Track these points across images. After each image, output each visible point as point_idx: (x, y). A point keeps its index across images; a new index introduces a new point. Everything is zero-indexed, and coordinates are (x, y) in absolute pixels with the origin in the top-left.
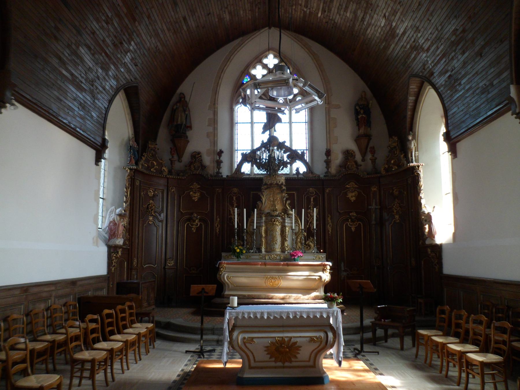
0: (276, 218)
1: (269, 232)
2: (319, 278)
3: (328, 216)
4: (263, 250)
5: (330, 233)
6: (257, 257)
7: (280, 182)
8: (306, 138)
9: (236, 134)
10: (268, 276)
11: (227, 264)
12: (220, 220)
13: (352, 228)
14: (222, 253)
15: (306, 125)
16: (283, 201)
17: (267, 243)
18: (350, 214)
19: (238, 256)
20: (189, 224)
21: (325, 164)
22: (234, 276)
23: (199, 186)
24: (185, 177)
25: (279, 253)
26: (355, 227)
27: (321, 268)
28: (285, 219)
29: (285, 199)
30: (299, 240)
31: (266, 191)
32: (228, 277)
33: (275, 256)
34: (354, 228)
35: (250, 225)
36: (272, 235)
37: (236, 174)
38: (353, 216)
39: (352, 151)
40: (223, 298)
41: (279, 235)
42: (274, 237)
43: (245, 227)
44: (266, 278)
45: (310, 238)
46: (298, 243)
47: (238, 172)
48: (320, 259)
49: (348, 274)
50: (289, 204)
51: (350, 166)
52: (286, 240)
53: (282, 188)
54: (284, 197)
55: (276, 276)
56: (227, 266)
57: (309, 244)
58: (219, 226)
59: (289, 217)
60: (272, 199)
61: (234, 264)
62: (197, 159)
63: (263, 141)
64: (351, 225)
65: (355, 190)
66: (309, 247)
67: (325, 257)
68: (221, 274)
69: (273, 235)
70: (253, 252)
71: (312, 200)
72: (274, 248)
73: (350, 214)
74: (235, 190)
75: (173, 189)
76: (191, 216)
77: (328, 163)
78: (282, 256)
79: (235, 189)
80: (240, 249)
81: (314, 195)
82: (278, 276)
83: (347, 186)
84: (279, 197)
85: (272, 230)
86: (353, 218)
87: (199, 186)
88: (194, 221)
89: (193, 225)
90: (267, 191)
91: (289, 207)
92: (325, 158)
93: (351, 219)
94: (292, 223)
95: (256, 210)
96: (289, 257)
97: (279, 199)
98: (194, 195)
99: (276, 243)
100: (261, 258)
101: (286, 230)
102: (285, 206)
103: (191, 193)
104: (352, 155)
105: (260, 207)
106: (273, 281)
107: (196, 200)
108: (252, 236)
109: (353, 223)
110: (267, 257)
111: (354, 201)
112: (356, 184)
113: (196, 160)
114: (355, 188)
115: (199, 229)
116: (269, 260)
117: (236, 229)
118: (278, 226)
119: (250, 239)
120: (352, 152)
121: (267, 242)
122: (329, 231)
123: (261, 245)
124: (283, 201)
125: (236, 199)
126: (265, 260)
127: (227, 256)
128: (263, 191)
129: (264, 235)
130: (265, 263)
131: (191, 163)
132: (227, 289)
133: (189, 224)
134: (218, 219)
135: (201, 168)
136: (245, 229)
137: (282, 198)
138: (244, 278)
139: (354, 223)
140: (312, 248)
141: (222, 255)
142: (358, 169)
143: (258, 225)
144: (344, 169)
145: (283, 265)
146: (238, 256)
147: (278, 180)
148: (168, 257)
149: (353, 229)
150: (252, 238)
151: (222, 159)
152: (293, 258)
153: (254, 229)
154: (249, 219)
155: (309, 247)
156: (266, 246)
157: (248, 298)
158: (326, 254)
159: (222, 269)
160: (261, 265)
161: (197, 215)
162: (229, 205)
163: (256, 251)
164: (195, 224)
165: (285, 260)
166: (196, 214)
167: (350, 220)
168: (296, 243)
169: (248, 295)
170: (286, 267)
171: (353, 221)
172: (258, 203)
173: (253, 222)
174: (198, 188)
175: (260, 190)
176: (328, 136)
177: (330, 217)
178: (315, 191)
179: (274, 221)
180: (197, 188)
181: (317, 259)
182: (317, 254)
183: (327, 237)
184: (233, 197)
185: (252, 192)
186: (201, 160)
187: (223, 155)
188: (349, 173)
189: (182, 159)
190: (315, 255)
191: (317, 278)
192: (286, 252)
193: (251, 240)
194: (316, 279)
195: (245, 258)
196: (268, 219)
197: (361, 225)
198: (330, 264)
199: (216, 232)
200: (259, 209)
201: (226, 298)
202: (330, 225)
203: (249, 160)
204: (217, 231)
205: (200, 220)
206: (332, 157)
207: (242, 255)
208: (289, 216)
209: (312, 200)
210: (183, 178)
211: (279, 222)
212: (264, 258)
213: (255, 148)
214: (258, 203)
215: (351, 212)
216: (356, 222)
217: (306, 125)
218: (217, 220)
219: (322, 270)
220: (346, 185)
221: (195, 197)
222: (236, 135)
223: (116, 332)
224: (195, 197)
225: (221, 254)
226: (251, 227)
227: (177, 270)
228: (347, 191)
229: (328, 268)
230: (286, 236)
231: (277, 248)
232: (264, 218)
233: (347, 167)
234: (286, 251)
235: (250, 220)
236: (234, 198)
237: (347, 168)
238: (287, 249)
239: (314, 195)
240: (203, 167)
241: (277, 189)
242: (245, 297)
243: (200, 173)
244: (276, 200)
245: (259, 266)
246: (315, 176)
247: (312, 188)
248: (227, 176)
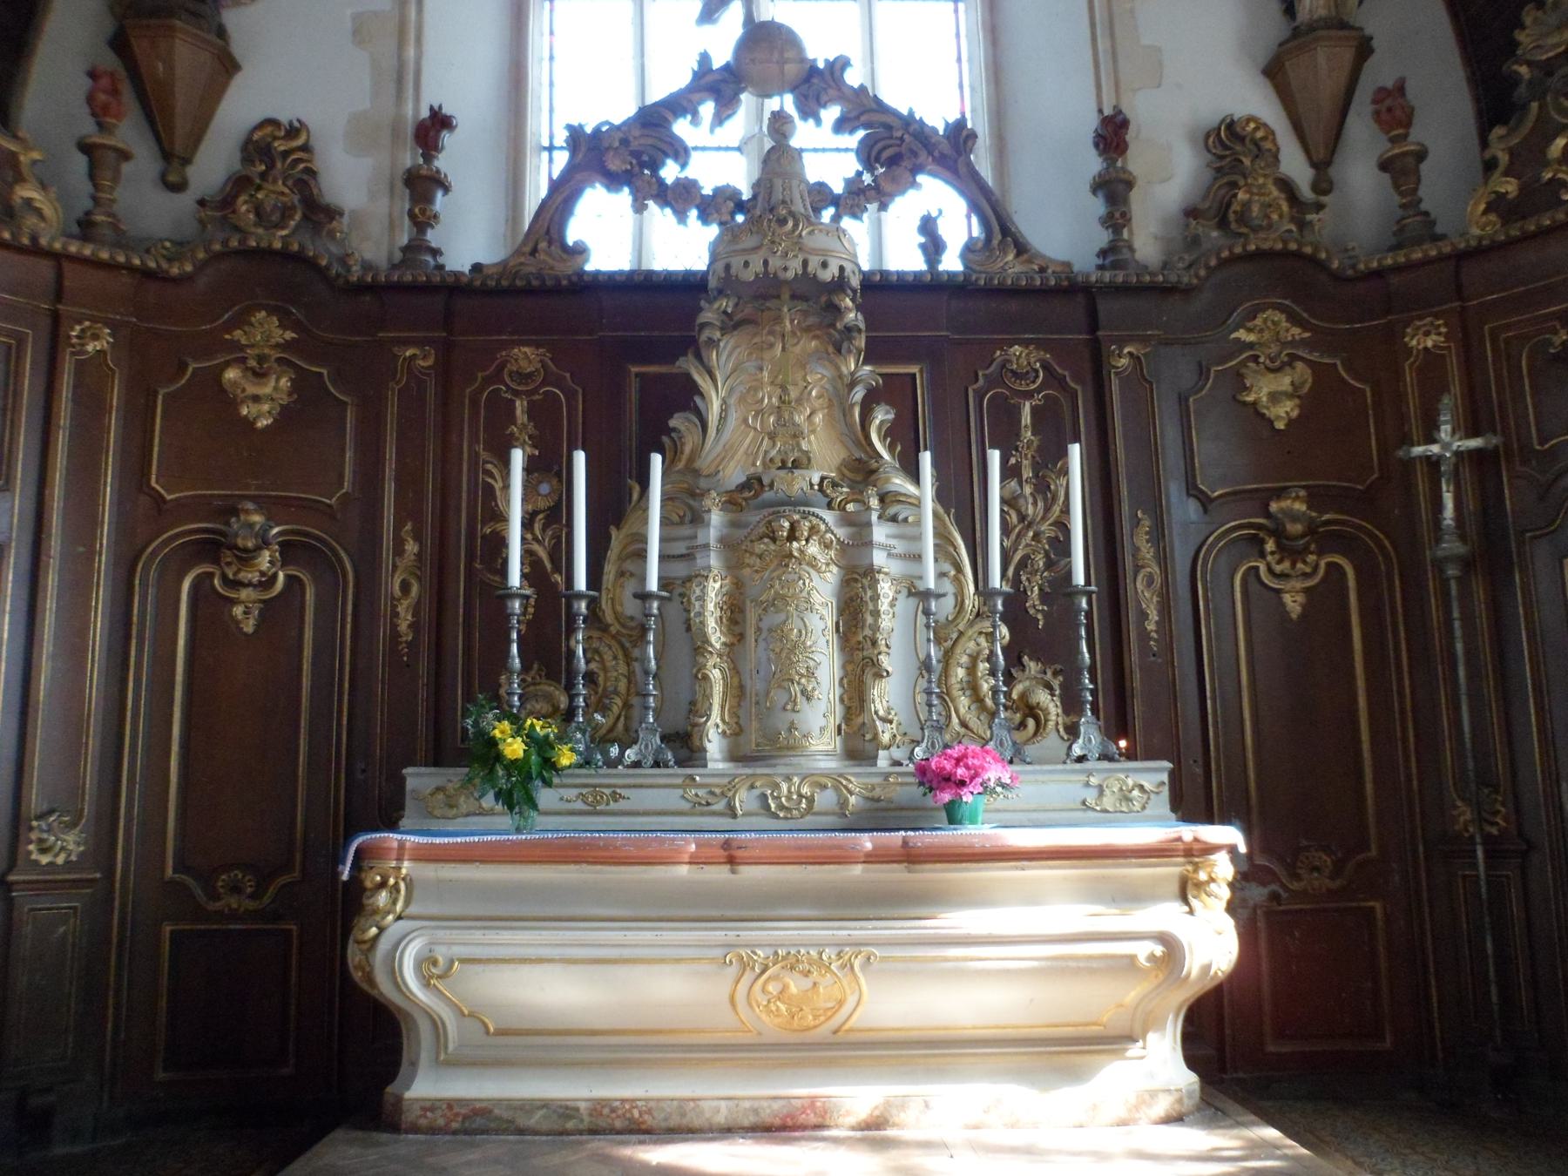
0: (805, 516)
1: (752, 615)
2: (1159, 950)
3: (1137, 522)
4: (714, 745)
5: (1151, 627)
6: (671, 798)
7: (825, 265)
8: (961, 86)
9: (546, 55)
10: (753, 946)
11: (427, 856)
12: (419, 556)
13: (1287, 598)
14: (408, 771)
15: (956, 11)
16: (846, 412)
17: (737, 692)
18: (1274, 507)
19: (517, 798)
20: (211, 575)
21: (1098, 206)
22: (478, 952)
23: (289, 335)
24: (189, 268)
25: (831, 764)
26: (1307, 591)
27: (1171, 870)
28: (869, 524)
29: (859, 394)
30: (961, 673)
31: (727, 343)
32: (426, 963)
33: (805, 790)
34: (1300, 598)
35: (621, 574)
36: (779, 632)
37: (534, 251)
38: (1295, 517)
39: (1256, 129)
40: (395, 1127)
41: (832, 636)
42: (792, 650)
43: (581, 583)
44: (733, 970)
45: (1023, 667)
46: (956, 693)
47: (543, 245)
48: (1129, 800)
49: (1274, 897)
50: (890, 433)
51: (1255, 209)
52: (880, 674)
53: (835, 310)
54: (852, 385)
55: (821, 945)
56: (429, 871)
57: (1033, 700)
58: (415, 589)
59: (894, 519)
60: (769, 398)
61: (483, 861)
62: (279, 165)
63: (705, 59)
64: (1283, 576)
65: (1293, 358)
66: (1031, 723)
67: (1166, 790)
68: (377, 937)
69: (784, 637)
70: (637, 764)
71: (1026, 417)
72: (792, 727)
73: (1274, 507)
74: (527, 357)
75: (96, 337)
76: (228, 524)
77: (1117, 218)
78: (855, 784)
79: (526, 349)
80: (531, 739)
81: (1038, 390)
82: (840, 945)
83: (1242, 334)
84: (818, 378)
85: (779, 602)
86: (1295, 528)
87: (289, 335)
88: (246, 557)
89: (237, 584)
90: (732, 342)
91: (891, 449)
92: (1094, 164)
93: (1278, 533)
94: (918, 558)
95: (657, 460)
96: (910, 791)
97: (819, 397)
98: (252, 390)
99: (804, 692)
100: (700, 807)
101: (876, 598)
102: (858, 443)
103: (231, 374)
104: (1259, 148)
105: (687, 449)
106: (793, 989)
107: (263, 423)
108: (636, 653)
109: (1293, 565)
110: (744, 799)
111: (1291, 423)
112: (1294, 319)
113: (271, 166)
114: (1293, 343)
115: (281, 611)
116: (764, 822)
117: (513, 596)
118: (819, 571)
119: (623, 668)
120: (1259, 134)
121: (741, 687)
122: (1143, 616)
123: (696, 708)
124: (846, 412)
125: (532, 412)
126: (725, 822)
127: (439, 789)
128: (712, 343)
129: (716, 637)
130: (726, 845)
131: (240, 183)
132: (425, 1057)
133: (211, 575)
134: (411, 547)
135: (305, 217)
136: (580, 596)
137: (837, 401)
138: (558, 968)
139: (1300, 565)
140: (1051, 724)
141: (411, 783)
142: (1302, 225)
143: (679, 569)
144: (1215, 234)
145: (872, 858)
146: (517, 798)
147: (816, 252)
148: (35, 799)
149: (1293, 603)
150: (636, 666)
151: (442, 163)
152: (946, 797)
153: (644, 597)
154: (614, 532)
155: (1031, 723)
156: (734, 714)
157: (594, 1131)
158: (1168, 765)
159: (383, 898)
160: (694, 861)
161: (268, 519)
162: (484, 455)
163: (658, 751)
164: (254, 577)
165: (878, 816)
166: (259, 510)
167: (1270, 546)
168: (945, 697)
169: (599, 1106)
170: (895, 874)
171: (1288, 550)
172: (672, 423)
173: (642, 555)
174: (287, 346)
175: (690, 344)
176: (1102, 44)
177: (1146, 524)
178: (1046, 366)
179: (792, 536)
180: (277, 345)
181: (1108, 802)
182: (1106, 765)
183: (1134, 657)
184: (513, 402)
185: (634, 369)
186: (312, 173)
187: (447, 138)
188: (1252, 247)
189: (192, 172)
190: (1090, 773)
191: (1144, 950)
192: (883, 762)
193: (630, 677)
194: (1132, 959)
195: (579, 805)
196: (746, 526)
197: (1343, 574)
198: (1230, 835)
199: (394, 626)
200: (681, 465)
201: (415, 1129)
202: (1150, 581)
203: (615, 165)
204: (403, 627)
205: (290, 551)
206: (1136, 161)
207: (547, 783)
208: (892, 511)
209: (1026, 417)
210: (175, 271)
211: (827, 546)
212: (720, 806)
213: (656, 94)
214: (672, 423)
215: (1279, 493)
216: (1311, 558)
217: (956, 11)
218: (399, 550)
219: (1175, 887)
220: (1236, 329)
221: (256, 399)
222: (546, 63)
223: (1415, 438)
224: (256, 399)
225: (403, 780)
226: (630, 587)
227: (110, 899)
228: (1243, 364)
229: (1223, 868)
230: (874, 643)
231: (816, 732)
232: (716, 518)
233: (1232, 217)
234: (881, 753)
235: (617, 538)
236: (520, 406)
237: (1233, 226)
238: (885, 738)
239: (1038, 390)
240: (319, 213)
241: (808, 329)
242: (570, 1125)
243: (296, 247)
244: (799, 401)
245: (683, 870)
246: (1042, 270)
247: (1025, 343)
248: (477, 268)
